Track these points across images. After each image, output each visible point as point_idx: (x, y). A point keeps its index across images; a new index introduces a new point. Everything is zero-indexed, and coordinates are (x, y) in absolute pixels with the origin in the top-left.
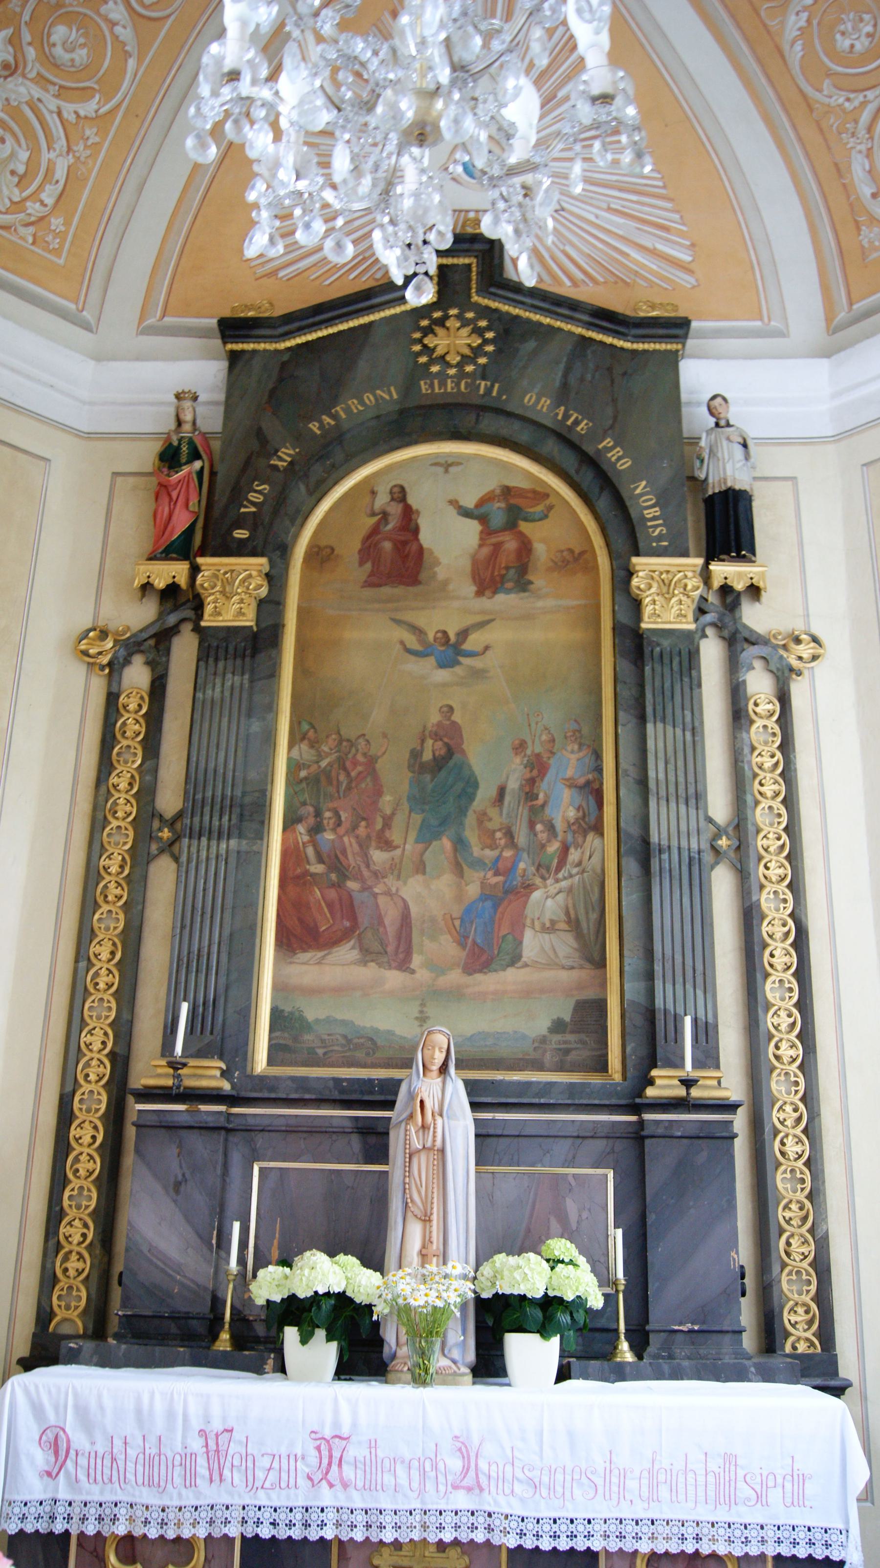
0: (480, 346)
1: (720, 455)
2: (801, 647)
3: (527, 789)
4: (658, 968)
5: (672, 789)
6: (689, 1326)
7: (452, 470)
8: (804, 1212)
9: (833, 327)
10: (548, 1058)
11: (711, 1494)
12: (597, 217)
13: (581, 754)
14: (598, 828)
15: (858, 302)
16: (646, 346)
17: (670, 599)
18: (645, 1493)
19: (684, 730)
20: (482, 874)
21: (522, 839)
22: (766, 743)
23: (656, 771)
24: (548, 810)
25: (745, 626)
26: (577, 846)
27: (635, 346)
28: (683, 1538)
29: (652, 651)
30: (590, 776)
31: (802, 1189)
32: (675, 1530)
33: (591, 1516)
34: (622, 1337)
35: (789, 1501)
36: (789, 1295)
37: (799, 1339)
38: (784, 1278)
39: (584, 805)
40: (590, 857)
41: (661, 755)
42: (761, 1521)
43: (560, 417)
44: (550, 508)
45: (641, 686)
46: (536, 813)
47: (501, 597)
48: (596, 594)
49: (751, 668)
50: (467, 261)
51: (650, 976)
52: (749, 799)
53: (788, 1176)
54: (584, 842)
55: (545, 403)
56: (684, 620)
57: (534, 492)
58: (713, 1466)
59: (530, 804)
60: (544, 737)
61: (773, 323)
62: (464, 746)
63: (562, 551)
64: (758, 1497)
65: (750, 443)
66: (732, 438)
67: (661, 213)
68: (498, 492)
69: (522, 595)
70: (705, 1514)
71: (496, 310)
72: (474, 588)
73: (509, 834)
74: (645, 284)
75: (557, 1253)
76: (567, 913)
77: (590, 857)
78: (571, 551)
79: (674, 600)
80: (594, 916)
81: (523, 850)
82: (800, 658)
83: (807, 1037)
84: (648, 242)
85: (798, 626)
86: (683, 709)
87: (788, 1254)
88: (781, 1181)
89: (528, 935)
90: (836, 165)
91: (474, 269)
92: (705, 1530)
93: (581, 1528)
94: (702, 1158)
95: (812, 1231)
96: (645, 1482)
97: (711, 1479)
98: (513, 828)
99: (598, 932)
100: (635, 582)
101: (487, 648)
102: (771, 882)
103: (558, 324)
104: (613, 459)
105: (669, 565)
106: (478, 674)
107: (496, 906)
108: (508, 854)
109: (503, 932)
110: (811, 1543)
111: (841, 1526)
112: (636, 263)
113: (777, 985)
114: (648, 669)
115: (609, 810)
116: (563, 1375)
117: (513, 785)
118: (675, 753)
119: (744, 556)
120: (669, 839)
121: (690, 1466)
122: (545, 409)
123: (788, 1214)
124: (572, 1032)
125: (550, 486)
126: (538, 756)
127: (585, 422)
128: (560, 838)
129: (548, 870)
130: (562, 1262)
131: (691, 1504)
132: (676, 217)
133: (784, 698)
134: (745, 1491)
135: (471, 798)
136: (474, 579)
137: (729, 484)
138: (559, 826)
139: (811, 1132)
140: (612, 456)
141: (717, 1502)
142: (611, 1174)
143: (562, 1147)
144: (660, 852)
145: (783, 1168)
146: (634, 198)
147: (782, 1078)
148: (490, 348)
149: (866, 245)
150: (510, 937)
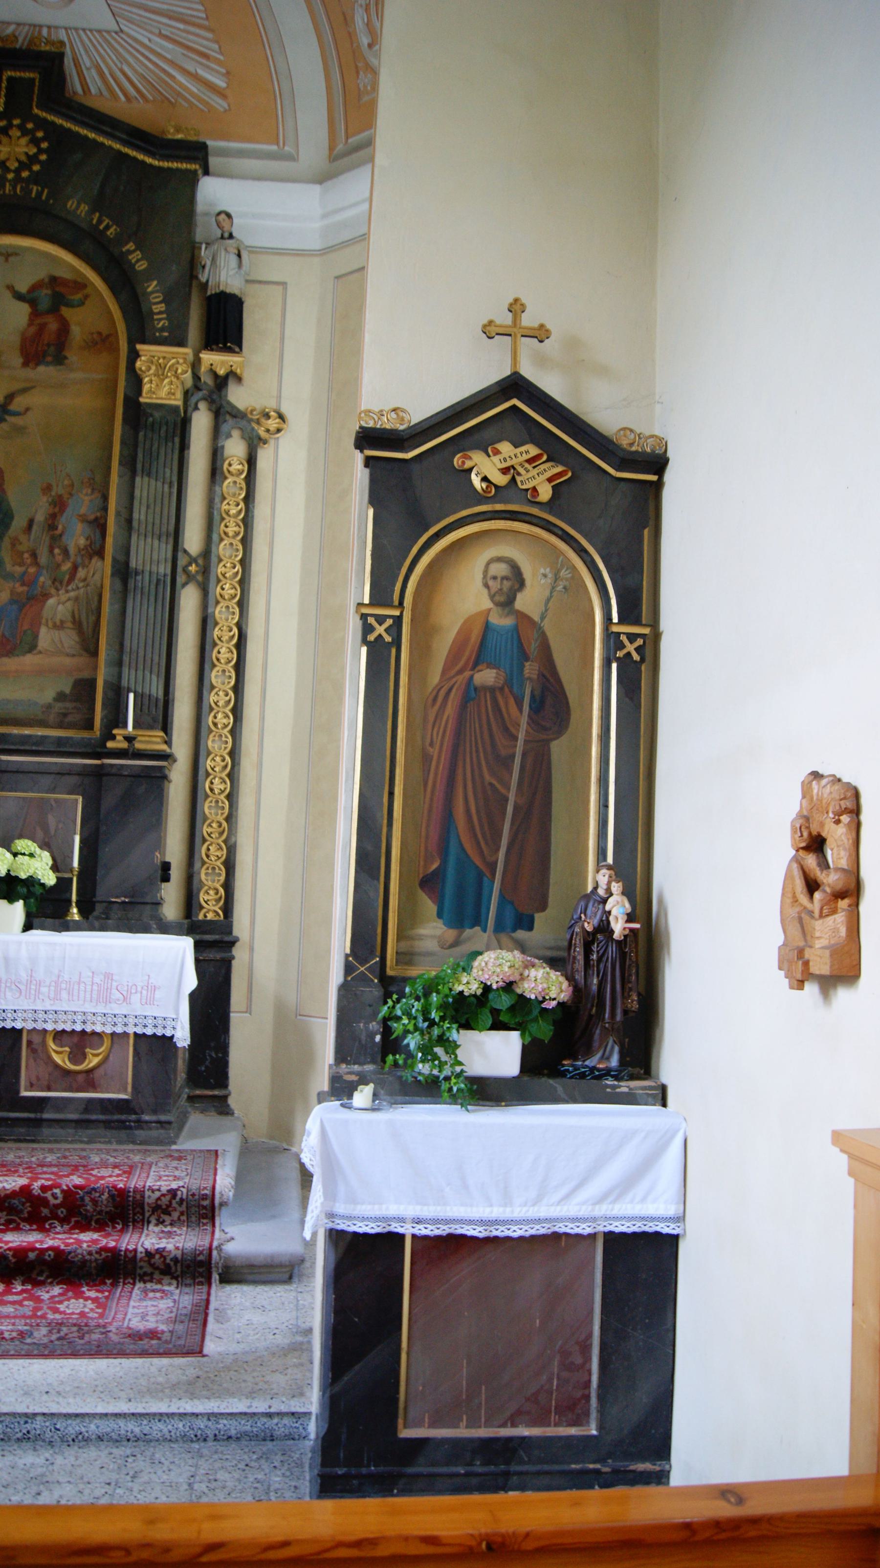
0: (36, 155)
1: (218, 263)
2: (270, 421)
3: (50, 522)
4: (126, 659)
5: (150, 528)
6: (123, 899)
7: (11, 259)
8: (222, 829)
9: (334, 156)
10: (52, 718)
11: (95, 996)
12: (150, 40)
13: (93, 497)
14: (100, 553)
15: (354, 135)
16: (170, 165)
17: (163, 380)
18: (52, 995)
19: (163, 483)
20: (11, 585)
21: (43, 559)
22: (234, 495)
23: (139, 514)
24: (64, 538)
25: (229, 403)
26: (84, 566)
27: (161, 164)
28: (74, 1022)
29: (146, 421)
30: (98, 514)
31: (222, 814)
32: (70, 1017)
33: (16, 1008)
34: (74, 904)
35: (144, 1001)
36: (205, 882)
37: (208, 911)
38: (203, 871)
39: (92, 536)
40: (94, 574)
41: (144, 501)
42: (125, 1013)
43: (95, 222)
44: (86, 297)
45: (136, 446)
46: (55, 540)
47: (41, 369)
48: (116, 368)
49: (229, 436)
50: (32, 75)
51: (120, 664)
52: (215, 537)
53: (213, 804)
54: (90, 563)
55: (84, 208)
56: (173, 397)
57: (75, 282)
58: (97, 980)
59: (52, 533)
60: (66, 482)
61: (286, 148)
62: (5, 487)
63: (92, 334)
64: (125, 999)
65: (244, 255)
66: (228, 249)
67: (204, 41)
68: (47, 280)
69: (59, 367)
70: (89, 1008)
71: (53, 123)
72: (21, 360)
73: (34, 555)
74: (186, 105)
75: (19, 848)
76: (73, 616)
77: (94, 574)
78: (100, 334)
79: (166, 381)
80: (92, 618)
81: (43, 567)
82: (268, 431)
83: (237, 711)
84: (190, 67)
85: (270, 404)
86: (165, 467)
87: (208, 856)
88: (207, 808)
89: (43, 630)
90: (344, 14)
91: (37, 84)
92: (90, 1017)
93: (9, 1015)
94: (141, 790)
95: (225, 842)
96: (52, 988)
97: (95, 987)
98: (38, 552)
99: (94, 631)
100: (138, 364)
101: (27, 409)
102: (224, 599)
103: (101, 139)
104: (133, 261)
105: (165, 352)
106: (20, 430)
107: (20, 610)
108: (32, 570)
109: (26, 627)
110: (155, 1026)
111: (174, 1016)
112: (181, 85)
113: (220, 673)
114: (141, 434)
115: (109, 540)
116: (28, 927)
117: (40, 517)
118: (155, 501)
119: (230, 347)
120: (143, 566)
121: (82, 980)
122: (83, 214)
123: (210, 830)
124: (71, 701)
125: (88, 279)
126: (60, 497)
127: (114, 227)
128: (72, 560)
129: (61, 583)
130: (24, 854)
131: (81, 1002)
132: (216, 46)
133: (251, 461)
134: (116, 995)
135: (7, 526)
136: (22, 354)
137: (222, 288)
138: (72, 550)
139: (233, 776)
140: (133, 258)
141: (98, 1001)
142: (80, 799)
143: (46, 781)
144: (137, 573)
145: (210, 799)
146: (181, 26)
147: (217, 738)
148: (43, 157)
149: (362, 89)
150: (29, 632)
